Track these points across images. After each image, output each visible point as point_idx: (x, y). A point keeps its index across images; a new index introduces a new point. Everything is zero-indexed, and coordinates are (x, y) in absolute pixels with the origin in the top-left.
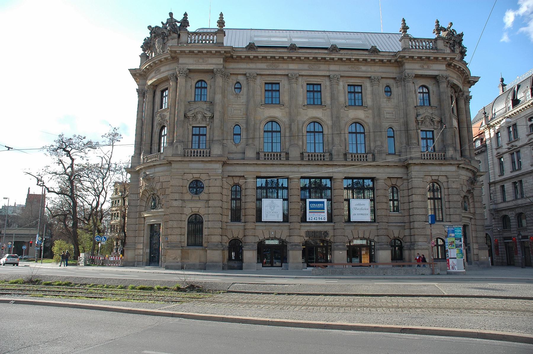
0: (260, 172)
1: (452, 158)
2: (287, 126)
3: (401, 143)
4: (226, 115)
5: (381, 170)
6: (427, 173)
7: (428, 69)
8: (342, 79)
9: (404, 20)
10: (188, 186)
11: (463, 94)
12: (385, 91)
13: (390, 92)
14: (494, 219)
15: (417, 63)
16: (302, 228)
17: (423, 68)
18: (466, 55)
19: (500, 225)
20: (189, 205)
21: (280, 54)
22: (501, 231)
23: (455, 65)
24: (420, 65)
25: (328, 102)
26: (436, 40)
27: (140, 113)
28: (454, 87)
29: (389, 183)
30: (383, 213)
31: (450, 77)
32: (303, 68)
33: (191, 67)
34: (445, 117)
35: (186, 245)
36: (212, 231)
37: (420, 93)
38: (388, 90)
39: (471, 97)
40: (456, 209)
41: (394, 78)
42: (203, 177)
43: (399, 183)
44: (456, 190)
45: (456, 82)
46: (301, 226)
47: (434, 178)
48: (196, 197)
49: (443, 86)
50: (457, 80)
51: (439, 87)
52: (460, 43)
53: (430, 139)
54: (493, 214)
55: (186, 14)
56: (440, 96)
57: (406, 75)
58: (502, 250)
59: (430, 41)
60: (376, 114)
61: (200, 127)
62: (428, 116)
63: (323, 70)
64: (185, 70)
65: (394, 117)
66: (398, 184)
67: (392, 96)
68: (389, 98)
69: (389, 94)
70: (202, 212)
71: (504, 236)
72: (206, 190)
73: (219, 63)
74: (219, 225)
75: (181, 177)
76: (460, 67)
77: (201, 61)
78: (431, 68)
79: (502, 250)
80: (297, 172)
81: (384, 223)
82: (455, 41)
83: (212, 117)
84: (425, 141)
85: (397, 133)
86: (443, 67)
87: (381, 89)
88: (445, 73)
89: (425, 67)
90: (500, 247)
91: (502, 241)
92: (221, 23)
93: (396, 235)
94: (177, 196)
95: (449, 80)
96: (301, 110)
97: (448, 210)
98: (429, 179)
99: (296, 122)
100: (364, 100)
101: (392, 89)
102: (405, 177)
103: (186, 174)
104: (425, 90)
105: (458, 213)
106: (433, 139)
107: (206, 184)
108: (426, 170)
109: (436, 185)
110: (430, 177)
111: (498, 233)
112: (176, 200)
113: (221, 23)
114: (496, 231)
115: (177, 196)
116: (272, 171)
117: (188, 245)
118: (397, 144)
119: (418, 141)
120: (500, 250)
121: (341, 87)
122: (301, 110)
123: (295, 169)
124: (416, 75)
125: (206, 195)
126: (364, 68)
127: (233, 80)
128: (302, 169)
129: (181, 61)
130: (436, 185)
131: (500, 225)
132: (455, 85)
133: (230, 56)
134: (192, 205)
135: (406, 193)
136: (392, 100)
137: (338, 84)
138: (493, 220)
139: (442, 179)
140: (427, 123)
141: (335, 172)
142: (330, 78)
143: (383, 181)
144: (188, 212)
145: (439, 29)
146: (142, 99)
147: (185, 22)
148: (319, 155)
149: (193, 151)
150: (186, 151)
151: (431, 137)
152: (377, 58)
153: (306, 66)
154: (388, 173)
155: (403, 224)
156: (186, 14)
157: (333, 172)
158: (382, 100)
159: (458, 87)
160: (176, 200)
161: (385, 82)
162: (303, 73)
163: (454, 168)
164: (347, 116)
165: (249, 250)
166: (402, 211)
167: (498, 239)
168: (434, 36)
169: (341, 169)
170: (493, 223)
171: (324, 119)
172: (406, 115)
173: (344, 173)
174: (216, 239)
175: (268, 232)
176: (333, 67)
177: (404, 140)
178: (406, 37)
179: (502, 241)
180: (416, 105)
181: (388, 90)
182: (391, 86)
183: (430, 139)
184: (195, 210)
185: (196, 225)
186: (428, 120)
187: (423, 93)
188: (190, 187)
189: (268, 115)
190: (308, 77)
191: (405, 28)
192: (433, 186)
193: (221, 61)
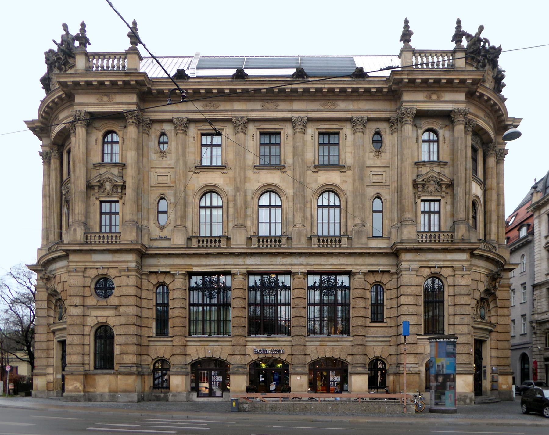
0: (192, 265)
1: (463, 241)
2: (231, 198)
3: (392, 221)
4: (146, 184)
5: (360, 261)
6: (424, 264)
7: (438, 101)
8: (310, 125)
9: (406, 21)
10: (93, 286)
11: (494, 147)
12: (374, 142)
13: (381, 142)
14: (535, 333)
15: (421, 91)
16: (249, 344)
17: (430, 100)
18: (504, 86)
19: (542, 342)
20: (94, 313)
21: (218, 85)
22: (542, 349)
23: (482, 95)
24: (425, 94)
25: (290, 161)
26: (454, 52)
27: (46, 188)
28: (478, 132)
29: (372, 279)
30: (360, 323)
31: (471, 113)
32: (255, 109)
33: (92, 109)
34: (458, 178)
35: (92, 368)
36: (124, 351)
37: (424, 141)
38: (378, 141)
39: (506, 152)
40: (463, 316)
41: (387, 120)
42: (112, 273)
43: (385, 279)
44: (465, 288)
45: (482, 123)
46: (247, 341)
47: (433, 270)
48: (103, 302)
49: (460, 128)
50: (484, 121)
51: (453, 131)
52: (494, 64)
53: (435, 212)
54: (534, 328)
55: (83, 25)
56: (453, 144)
57: (404, 112)
58: (542, 374)
59: (443, 55)
60: (357, 176)
61: (111, 202)
62: (432, 177)
63: (282, 110)
64: (83, 113)
65: (384, 181)
66: (384, 281)
67: (383, 147)
68: (162, 154)
69: (379, 145)
70: (111, 322)
71: (545, 356)
72: (116, 292)
73: (132, 101)
74: (134, 340)
75: (81, 274)
76: (489, 99)
77: (105, 99)
78: (443, 99)
79: (542, 374)
80: (243, 265)
81: (360, 337)
82: (481, 55)
83: (124, 187)
84: (427, 216)
85: (388, 205)
86: (462, 97)
87: (368, 138)
88: (462, 106)
89: (434, 97)
90: (539, 371)
91: (542, 363)
92: (134, 37)
93: (378, 354)
94: (77, 301)
95: (470, 120)
96: (250, 174)
97: (451, 317)
98: (426, 272)
99: (242, 192)
100: (342, 156)
101: (384, 136)
102: (393, 270)
103: (88, 270)
104: (433, 137)
105: (465, 322)
106: (439, 212)
107: (116, 282)
108: (423, 259)
109: (437, 281)
110: (95, 270)
111: (538, 353)
112: (76, 306)
113: (134, 37)
114: (535, 349)
115: (77, 301)
116: (208, 263)
117: (95, 368)
118: (386, 222)
119: (416, 217)
120: (539, 374)
121: (308, 137)
122: (250, 174)
123: (240, 261)
124: (418, 111)
125: (116, 299)
126: (342, 105)
127: (157, 129)
128: (250, 261)
129: (406, 97)
130: (437, 281)
131: (542, 342)
132: (482, 129)
133: (146, 91)
134: (99, 313)
135: (394, 293)
136: (383, 154)
137: (304, 133)
138: (534, 336)
139: (446, 272)
140: (432, 188)
141: (294, 265)
142: (293, 123)
143: (362, 276)
144: (91, 321)
145: (458, 36)
146: (47, 167)
147: (83, 40)
148: (273, 239)
149: (101, 235)
150: (89, 236)
151: (437, 209)
152: (362, 86)
153: (257, 105)
154: (368, 265)
155: (388, 339)
156: (83, 25)
157: (291, 265)
158: (367, 154)
159: (486, 132)
160: (76, 306)
161: (372, 127)
162: (253, 115)
163: (465, 256)
164: (316, 181)
165: (177, 373)
166: (388, 320)
167: (538, 360)
168: (452, 46)
169: (303, 260)
170: (534, 339)
171: (282, 185)
172: (400, 175)
173: (307, 265)
174: (130, 359)
175: (203, 349)
176: (297, 105)
177: (395, 215)
178: (407, 49)
179: (542, 363)
180: (416, 161)
181: (378, 141)
182: (383, 133)
183: (435, 212)
184: (101, 320)
185: (104, 335)
186: (432, 182)
187: (429, 141)
188: (96, 288)
189: (205, 183)
190: (262, 123)
191: (406, 36)
192: (433, 282)
193: (133, 98)
